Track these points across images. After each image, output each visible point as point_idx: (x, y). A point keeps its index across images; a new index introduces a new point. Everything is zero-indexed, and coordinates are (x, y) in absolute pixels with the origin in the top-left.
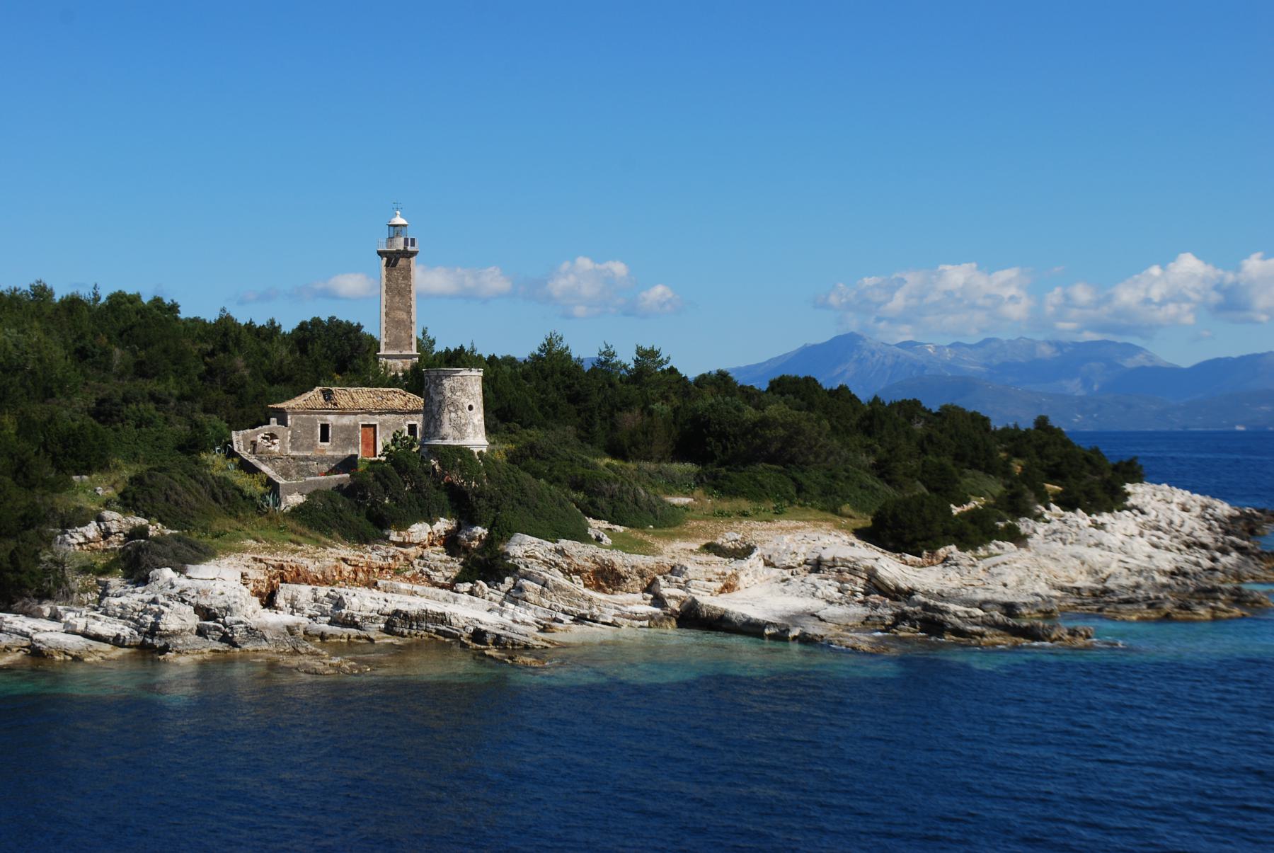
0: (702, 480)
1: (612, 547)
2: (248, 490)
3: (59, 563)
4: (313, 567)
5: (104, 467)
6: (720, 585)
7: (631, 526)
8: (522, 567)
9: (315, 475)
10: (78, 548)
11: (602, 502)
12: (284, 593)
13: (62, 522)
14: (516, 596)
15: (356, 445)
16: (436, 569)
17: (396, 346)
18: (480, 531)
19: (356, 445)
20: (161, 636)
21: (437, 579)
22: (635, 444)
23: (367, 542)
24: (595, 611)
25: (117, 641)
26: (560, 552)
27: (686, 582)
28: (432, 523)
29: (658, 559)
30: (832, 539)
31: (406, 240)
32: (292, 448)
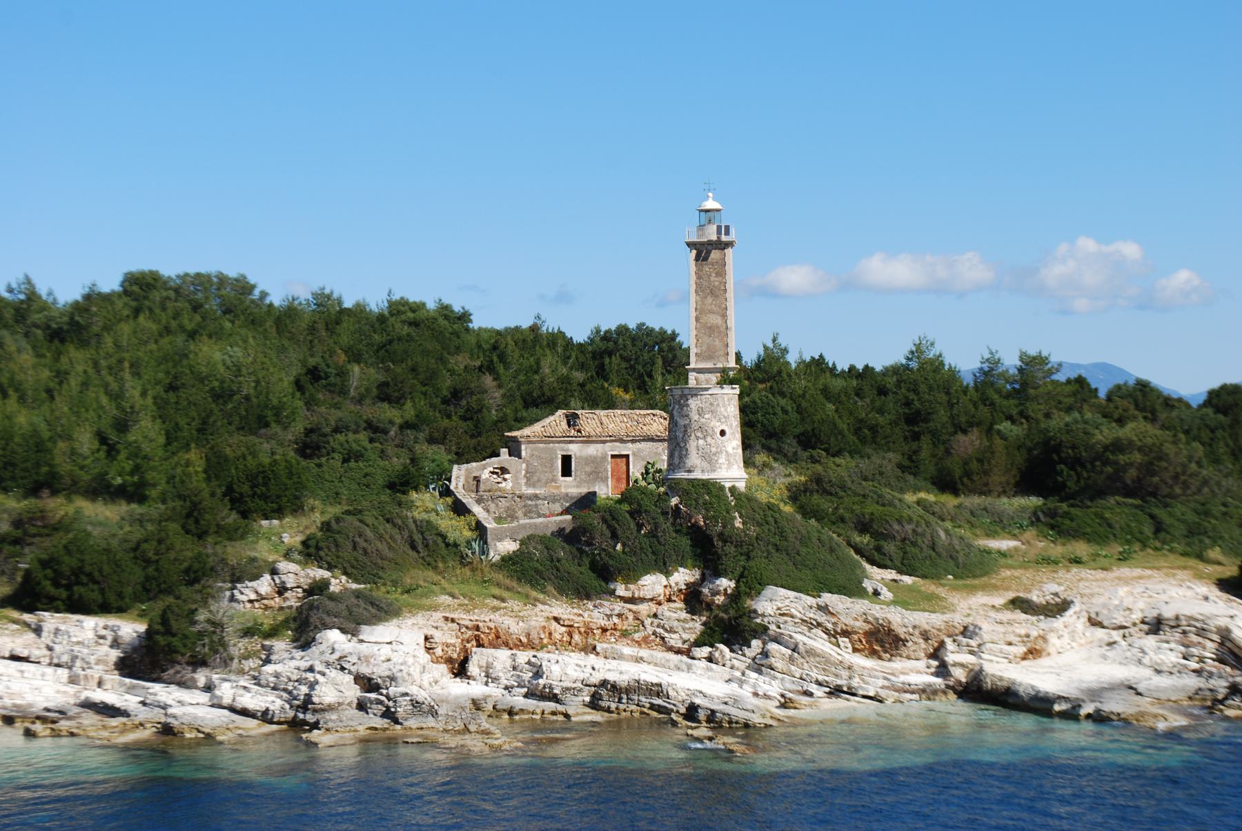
0: (1038, 520)
1: (894, 603)
2: (452, 537)
3: (217, 625)
4: (515, 627)
5: (297, 509)
6: (1022, 649)
7: (924, 577)
8: (773, 627)
9: (545, 516)
10: (248, 605)
11: (890, 547)
12: (479, 659)
13: (233, 575)
14: (761, 665)
15: (605, 480)
16: (671, 631)
17: (710, 358)
18: (725, 583)
19: (605, 480)
20: (315, 711)
21: (672, 643)
22: (968, 474)
23: (588, 597)
24: (856, 682)
25: (265, 717)
26: (824, 609)
27: (980, 645)
28: (668, 574)
29: (947, 617)
30: (1181, 591)
31: (719, 228)
32: (529, 483)
